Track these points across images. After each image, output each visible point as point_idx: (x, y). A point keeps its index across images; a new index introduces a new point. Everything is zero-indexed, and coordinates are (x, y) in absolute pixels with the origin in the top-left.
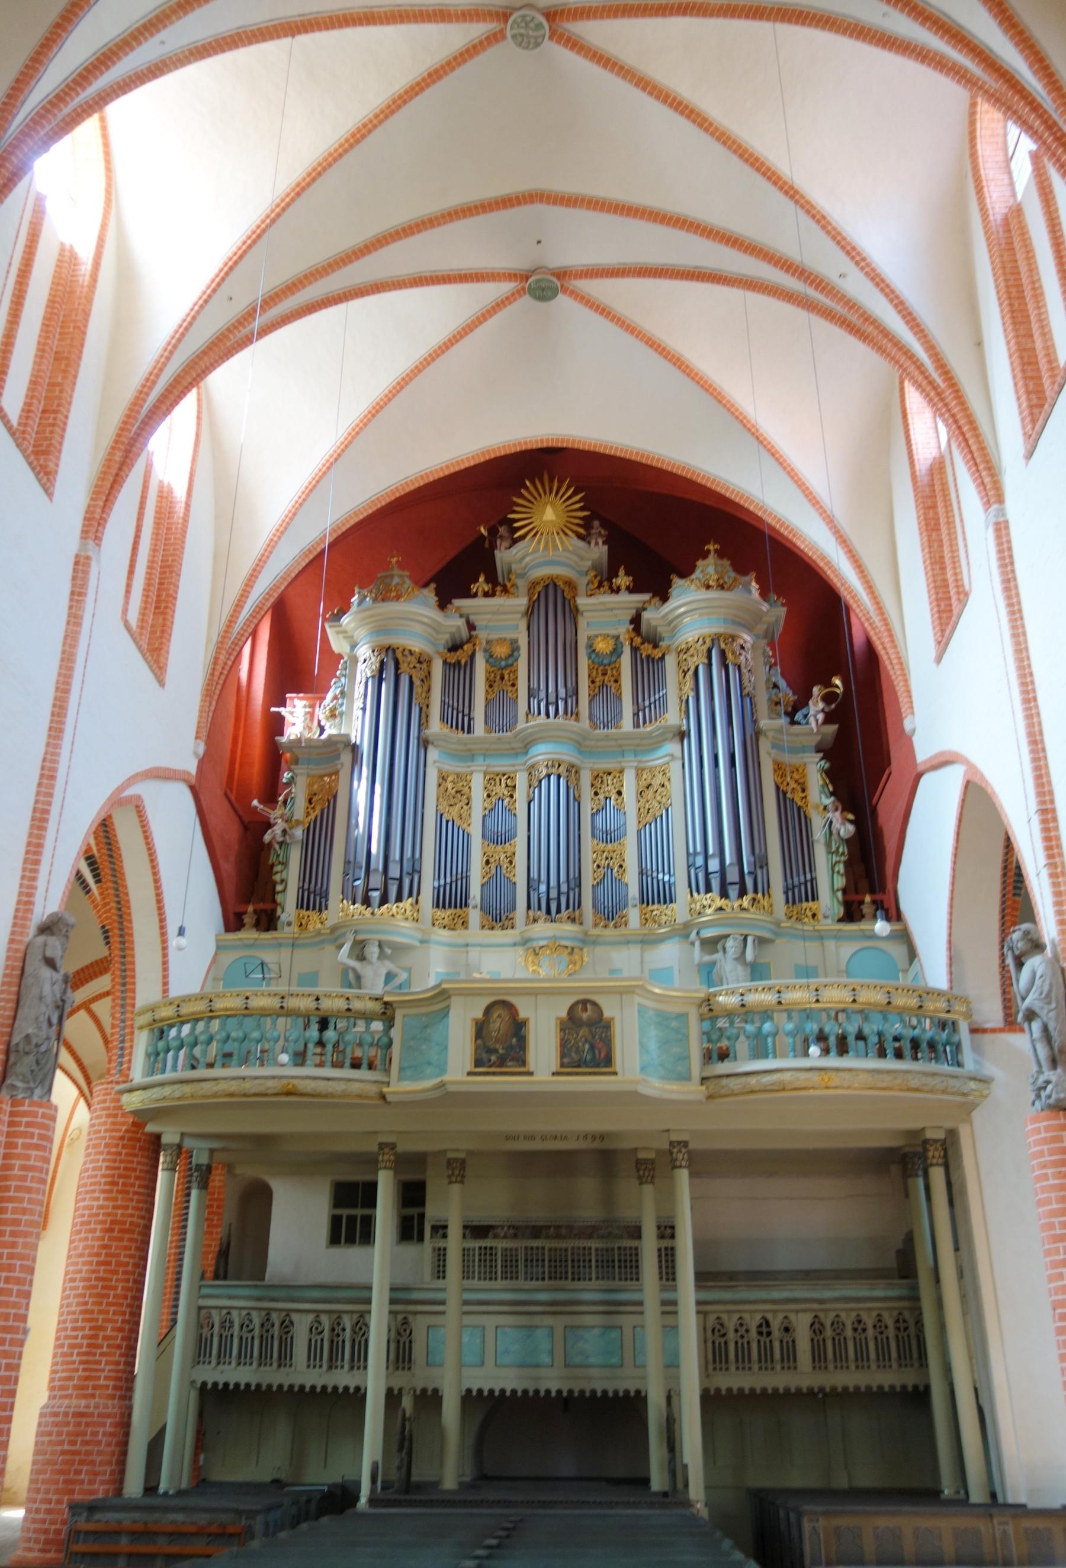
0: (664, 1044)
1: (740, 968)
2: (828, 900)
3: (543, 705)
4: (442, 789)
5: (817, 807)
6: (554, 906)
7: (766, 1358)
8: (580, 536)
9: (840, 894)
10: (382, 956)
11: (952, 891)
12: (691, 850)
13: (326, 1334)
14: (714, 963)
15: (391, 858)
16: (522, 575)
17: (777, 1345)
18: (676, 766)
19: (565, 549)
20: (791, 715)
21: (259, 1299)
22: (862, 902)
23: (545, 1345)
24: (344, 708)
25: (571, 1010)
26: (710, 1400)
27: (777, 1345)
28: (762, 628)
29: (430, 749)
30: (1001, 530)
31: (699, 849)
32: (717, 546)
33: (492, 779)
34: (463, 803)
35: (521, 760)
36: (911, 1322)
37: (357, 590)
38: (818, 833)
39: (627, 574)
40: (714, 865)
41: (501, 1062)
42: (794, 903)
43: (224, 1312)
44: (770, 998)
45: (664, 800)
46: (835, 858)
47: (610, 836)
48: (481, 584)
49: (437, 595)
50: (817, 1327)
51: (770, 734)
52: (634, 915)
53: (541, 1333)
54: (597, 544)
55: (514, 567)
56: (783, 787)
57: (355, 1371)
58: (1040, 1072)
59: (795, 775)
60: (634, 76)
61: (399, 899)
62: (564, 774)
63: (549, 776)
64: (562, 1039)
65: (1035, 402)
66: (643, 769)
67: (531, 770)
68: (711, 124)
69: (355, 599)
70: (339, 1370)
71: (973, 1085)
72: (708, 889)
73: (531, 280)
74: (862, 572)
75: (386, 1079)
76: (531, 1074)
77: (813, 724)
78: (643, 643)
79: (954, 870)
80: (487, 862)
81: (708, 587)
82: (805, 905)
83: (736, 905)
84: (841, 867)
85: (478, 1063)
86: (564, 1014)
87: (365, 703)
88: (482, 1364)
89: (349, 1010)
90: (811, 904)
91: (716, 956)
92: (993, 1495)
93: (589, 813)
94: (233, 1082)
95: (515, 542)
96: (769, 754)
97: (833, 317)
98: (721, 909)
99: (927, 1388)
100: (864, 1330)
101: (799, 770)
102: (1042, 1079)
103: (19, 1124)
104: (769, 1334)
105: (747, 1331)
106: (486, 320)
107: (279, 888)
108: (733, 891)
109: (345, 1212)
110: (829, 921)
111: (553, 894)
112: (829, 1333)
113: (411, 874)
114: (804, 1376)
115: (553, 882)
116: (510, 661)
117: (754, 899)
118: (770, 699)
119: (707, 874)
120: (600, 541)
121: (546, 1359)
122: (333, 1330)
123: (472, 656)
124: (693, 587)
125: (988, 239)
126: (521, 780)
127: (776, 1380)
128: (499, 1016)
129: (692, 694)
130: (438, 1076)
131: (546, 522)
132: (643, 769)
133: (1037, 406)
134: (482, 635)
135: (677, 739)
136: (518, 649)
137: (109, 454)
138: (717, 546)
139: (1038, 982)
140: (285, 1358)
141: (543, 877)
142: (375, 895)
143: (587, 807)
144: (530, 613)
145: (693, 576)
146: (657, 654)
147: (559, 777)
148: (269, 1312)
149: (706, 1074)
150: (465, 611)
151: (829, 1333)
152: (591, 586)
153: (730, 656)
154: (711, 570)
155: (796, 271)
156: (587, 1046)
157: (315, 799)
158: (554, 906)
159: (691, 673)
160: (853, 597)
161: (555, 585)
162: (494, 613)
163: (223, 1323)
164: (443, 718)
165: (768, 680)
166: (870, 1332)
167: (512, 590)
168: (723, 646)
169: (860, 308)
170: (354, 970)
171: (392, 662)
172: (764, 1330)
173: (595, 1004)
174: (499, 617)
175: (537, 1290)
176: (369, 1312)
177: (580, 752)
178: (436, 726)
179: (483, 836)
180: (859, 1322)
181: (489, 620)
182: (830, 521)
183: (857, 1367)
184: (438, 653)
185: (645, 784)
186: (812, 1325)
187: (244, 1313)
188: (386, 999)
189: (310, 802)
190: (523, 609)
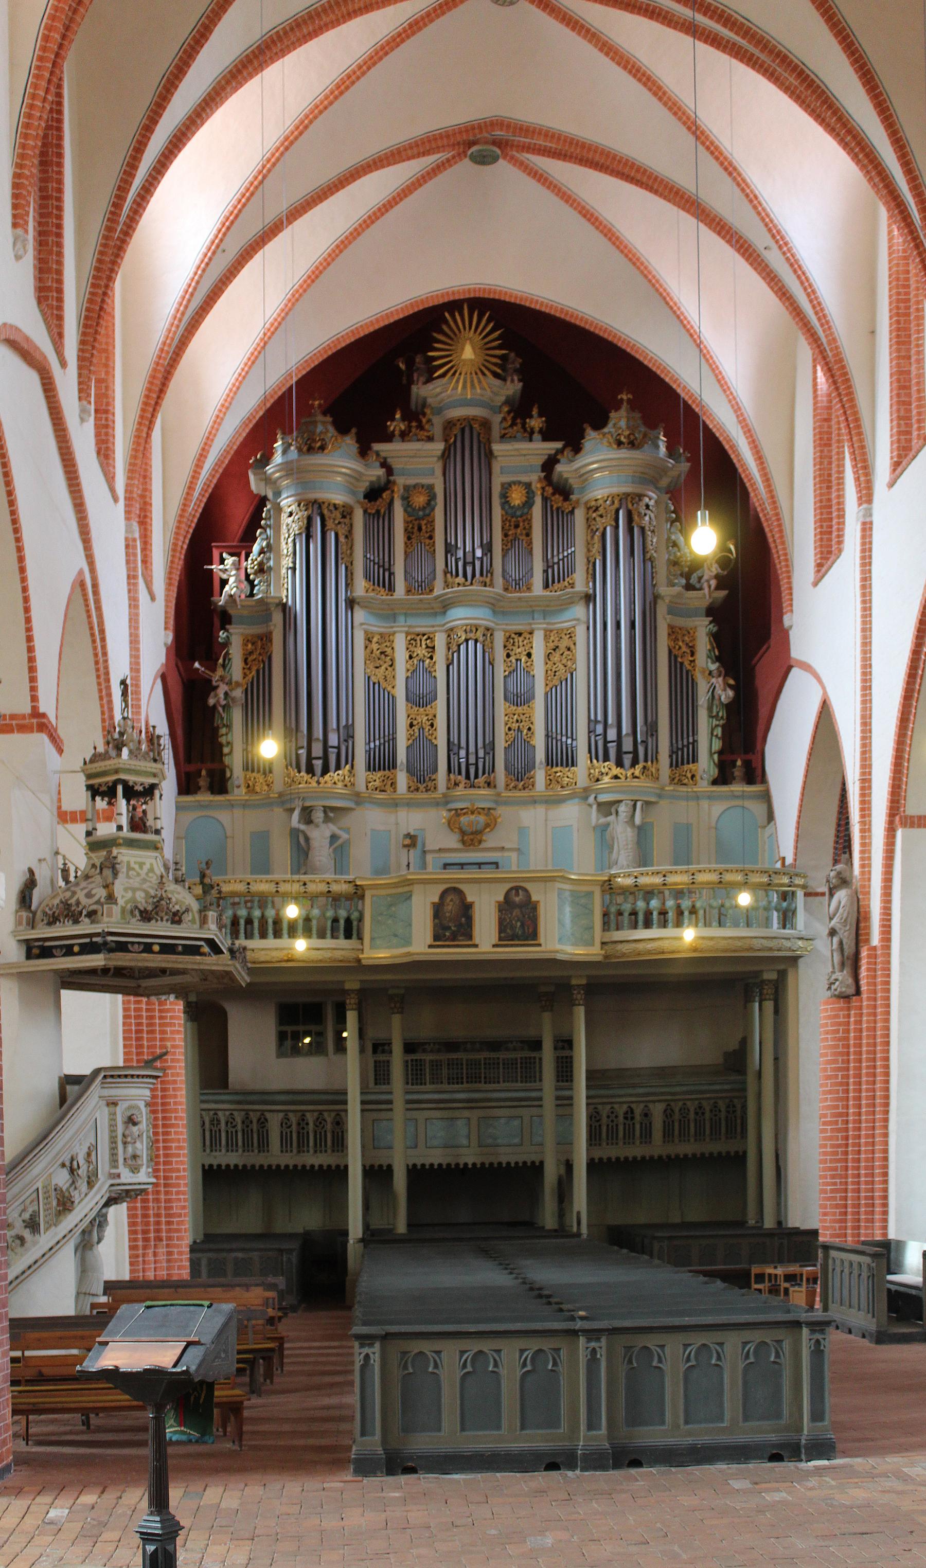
0: (575, 916)
1: (629, 829)
2: (705, 765)
3: (460, 564)
4: (368, 651)
6: (472, 770)
7: (629, 1137)
8: (496, 375)
9: (716, 757)
10: (327, 819)
11: (805, 782)
12: (592, 717)
13: (294, 1127)
14: (608, 825)
15: (330, 728)
16: (439, 411)
17: (638, 1127)
18: (580, 632)
21: (239, 1103)
23: (464, 1131)
24: (271, 563)
26: (593, 1166)
27: (638, 1127)
28: (664, 482)
29: (356, 608)
30: (867, 529)
31: (599, 718)
32: (630, 396)
33: (413, 639)
35: (439, 620)
36: (739, 1107)
38: (703, 699)
39: (540, 415)
40: (612, 734)
41: (454, 937)
42: (677, 766)
45: (569, 663)
46: (715, 722)
47: (520, 699)
48: (397, 425)
49: (357, 442)
50: (668, 1113)
52: (540, 776)
53: (460, 1123)
54: (512, 381)
55: (429, 400)
56: (675, 652)
58: (833, 972)
59: (686, 638)
60: (598, 40)
61: (338, 767)
62: (481, 639)
63: (467, 641)
64: (500, 919)
65: (903, 428)
67: (450, 632)
68: (664, 93)
69: (278, 444)
71: (800, 943)
76: (476, 946)
77: (706, 590)
78: (553, 494)
79: (808, 765)
80: (411, 725)
81: (619, 444)
82: (686, 767)
83: (629, 774)
84: (719, 731)
85: (436, 937)
86: (501, 898)
87: (294, 563)
88: (416, 1147)
89: (329, 892)
91: (611, 818)
92: (780, 1223)
95: (430, 379)
98: (616, 777)
99: (745, 1153)
100: (703, 1114)
101: (689, 632)
102: (834, 977)
103: (166, 1018)
104: (633, 1118)
107: (226, 750)
108: (627, 759)
111: (472, 760)
112: (677, 1116)
113: (346, 741)
114: (657, 1148)
116: (427, 512)
117: (644, 767)
119: (606, 742)
120: (516, 378)
121: (465, 1142)
122: (299, 1124)
123: (391, 504)
124: (605, 441)
125: (890, 254)
126: (440, 641)
127: (636, 1151)
130: (403, 946)
131: (465, 360)
133: (903, 456)
134: (401, 481)
135: (582, 603)
136: (432, 497)
138: (630, 396)
139: (841, 910)
140: (264, 1145)
141: (463, 744)
142: (318, 764)
144: (445, 456)
145: (606, 430)
147: (476, 641)
148: (247, 1112)
149: (605, 940)
150: (383, 454)
151: (677, 1116)
152: (505, 425)
153: (636, 518)
154: (623, 423)
157: (250, 659)
158: (472, 770)
160: (752, 485)
161: (471, 428)
163: (212, 1122)
164: (367, 577)
167: (427, 427)
168: (630, 506)
169: (780, 281)
170: (303, 832)
171: (317, 513)
172: (629, 1115)
173: (526, 890)
174: (417, 460)
175: (458, 1092)
178: (361, 586)
179: (407, 700)
180: (700, 1108)
182: (737, 409)
184: (358, 502)
185: (552, 645)
187: (228, 1113)
188: (358, 883)
189: (246, 661)
190: (439, 453)
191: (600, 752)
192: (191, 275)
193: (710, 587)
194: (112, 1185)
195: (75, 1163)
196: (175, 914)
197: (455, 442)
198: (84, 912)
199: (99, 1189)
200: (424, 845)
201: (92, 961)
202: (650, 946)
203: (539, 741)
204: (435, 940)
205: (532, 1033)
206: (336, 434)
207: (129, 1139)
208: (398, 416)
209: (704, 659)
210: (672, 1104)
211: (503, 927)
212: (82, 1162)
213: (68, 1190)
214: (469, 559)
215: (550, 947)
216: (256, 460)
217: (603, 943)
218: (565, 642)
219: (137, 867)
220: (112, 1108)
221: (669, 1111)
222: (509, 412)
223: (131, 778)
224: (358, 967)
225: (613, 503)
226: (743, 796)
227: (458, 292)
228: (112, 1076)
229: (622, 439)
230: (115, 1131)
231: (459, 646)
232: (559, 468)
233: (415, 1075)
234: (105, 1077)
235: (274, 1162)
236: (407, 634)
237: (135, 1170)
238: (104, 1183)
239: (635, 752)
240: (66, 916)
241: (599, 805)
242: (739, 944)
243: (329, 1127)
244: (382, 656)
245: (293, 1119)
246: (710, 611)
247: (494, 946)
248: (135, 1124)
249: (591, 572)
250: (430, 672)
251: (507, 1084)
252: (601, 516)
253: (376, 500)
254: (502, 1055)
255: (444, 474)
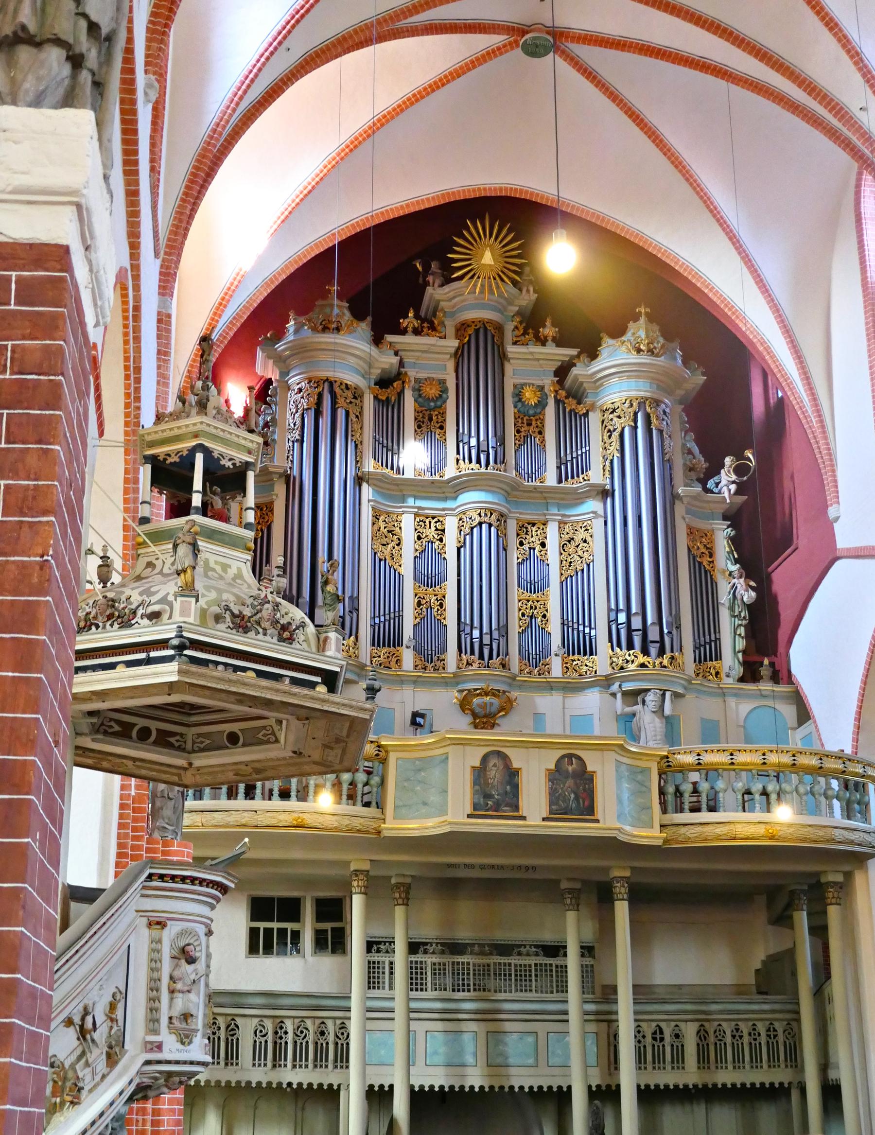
1: (657, 720)
2: (730, 660)
4: (376, 528)
5: (724, 571)
9: (740, 655)
12: (613, 606)
13: (270, 1037)
14: (634, 715)
16: (453, 314)
17: (668, 1049)
18: (598, 524)
19: (500, 295)
20: (703, 482)
22: (761, 664)
25: (559, 763)
27: (668, 1049)
28: (680, 392)
29: (365, 486)
31: (621, 606)
32: (648, 310)
33: (423, 519)
34: (393, 544)
37: (292, 315)
38: (724, 598)
40: (637, 623)
42: (700, 662)
43: (230, 1018)
44: (724, 758)
45: (586, 555)
46: (737, 622)
47: (537, 586)
48: (410, 321)
49: (372, 330)
50: (702, 1034)
51: (685, 500)
55: (442, 304)
56: (694, 552)
57: (229, 1067)
62: (495, 524)
63: (480, 524)
66: (565, 523)
70: (282, 1068)
72: (630, 646)
73: (527, 37)
74: (801, 362)
75: (380, 816)
77: (726, 495)
78: (567, 397)
80: (419, 604)
82: (709, 664)
83: (657, 662)
84: (742, 631)
85: (476, 807)
86: (552, 767)
87: (302, 437)
90: (714, 663)
91: (638, 708)
93: (515, 562)
94: (246, 814)
95: (448, 281)
96: (684, 518)
97: (838, 138)
98: (643, 665)
100: (741, 1037)
104: (662, 1039)
105: (644, 1037)
106: (474, 67)
108: (653, 650)
109: (262, 925)
110: (730, 680)
114: (690, 1075)
115: (485, 629)
116: (439, 403)
117: (672, 658)
118: (685, 464)
121: (470, 1059)
122: (276, 1033)
123: (400, 394)
124: (624, 348)
126: (451, 524)
128: (495, 765)
129: (617, 455)
132: (565, 523)
136: (445, 390)
137: (179, 206)
138: (648, 310)
141: (476, 623)
143: (514, 556)
144: (458, 355)
145: (624, 338)
146: (582, 410)
147: (490, 525)
151: (712, 1039)
152: (517, 333)
153: (654, 420)
154: (642, 334)
155: (818, 94)
156: (572, 796)
159: (616, 435)
161: (486, 329)
162: (423, 352)
165: (684, 445)
166: (746, 1039)
167: (439, 328)
172: (658, 1036)
173: (579, 758)
174: (429, 355)
176: (349, 1018)
177: (507, 501)
179: (415, 579)
180: (737, 1030)
181: (418, 358)
183: (734, 1067)
185: (567, 537)
186: (698, 1032)
190: (453, 350)
191: (624, 638)
192: (253, 62)
193: (730, 490)
194: (148, 1063)
195: (89, 1020)
196: (284, 628)
197: (469, 341)
198: (140, 612)
199: (126, 1069)
200: (431, 725)
201: (156, 674)
202: (720, 830)
203: (554, 628)
204: (475, 809)
205: (548, 937)
206: (352, 318)
207: (179, 986)
208: (411, 315)
209: (724, 560)
210: (706, 1024)
211: (554, 798)
212: (100, 1018)
213: (73, 1067)
214: (483, 447)
215: (609, 824)
216: (266, 338)
217: (661, 826)
218: (581, 534)
219: (218, 568)
220: (156, 932)
221: (702, 1033)
222: (521, 322)
223: (217, 448)
224: (378, 840)
225: (631, 405)
226: (774, 696)
227: (490, 189)
228: (162, 877)
229: (642, 347)
230: (158, 970)
231: (472, 529)
232: (575, 371)
233: (415, 981)
234: (150, 877)
235: (244, 1077)
236: (416, 515)
237: (185, 1039)
238: (133, 1058)
239: (662, 642)
240: (110, 617)
241: (625, 694)
242: (821, 833)
243: (311, 1038)
244: (388, 534)
245: (269, 1025)
246: (733, 517)
247: (544, 819)
248: (191, 961)
249: (608, 468)
250: (440, 555)
251: (519, 994)
252: (619, 417)
253: (387, 388)
254: (514, 960)
255: (457, 371)
